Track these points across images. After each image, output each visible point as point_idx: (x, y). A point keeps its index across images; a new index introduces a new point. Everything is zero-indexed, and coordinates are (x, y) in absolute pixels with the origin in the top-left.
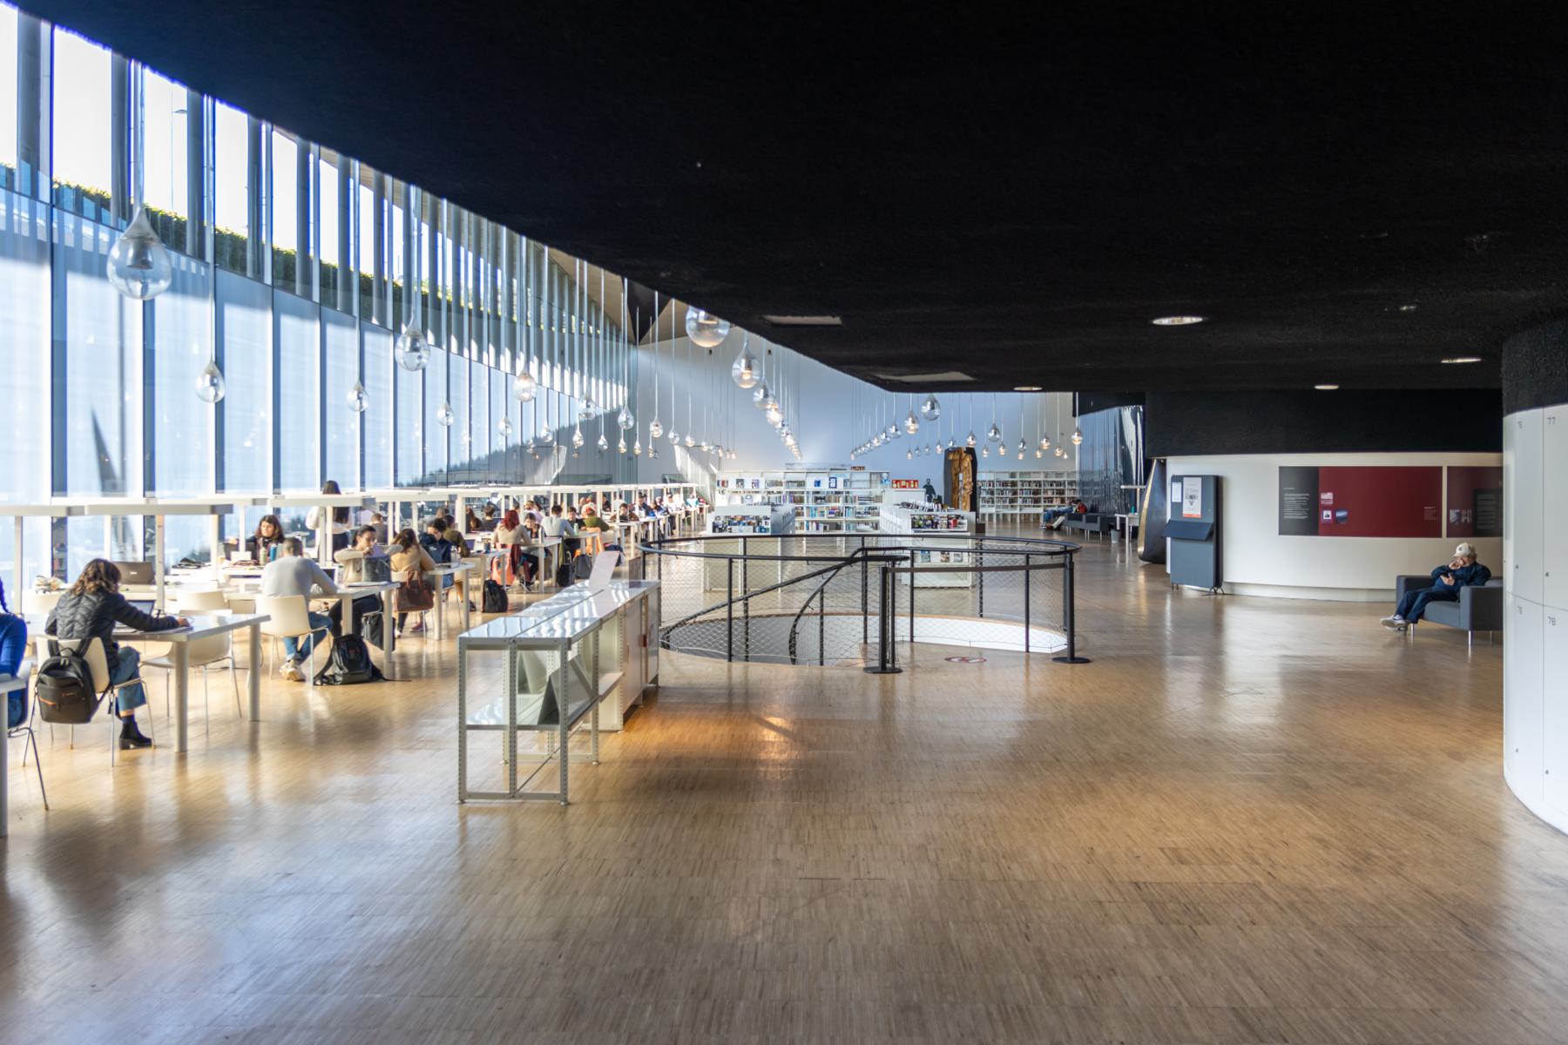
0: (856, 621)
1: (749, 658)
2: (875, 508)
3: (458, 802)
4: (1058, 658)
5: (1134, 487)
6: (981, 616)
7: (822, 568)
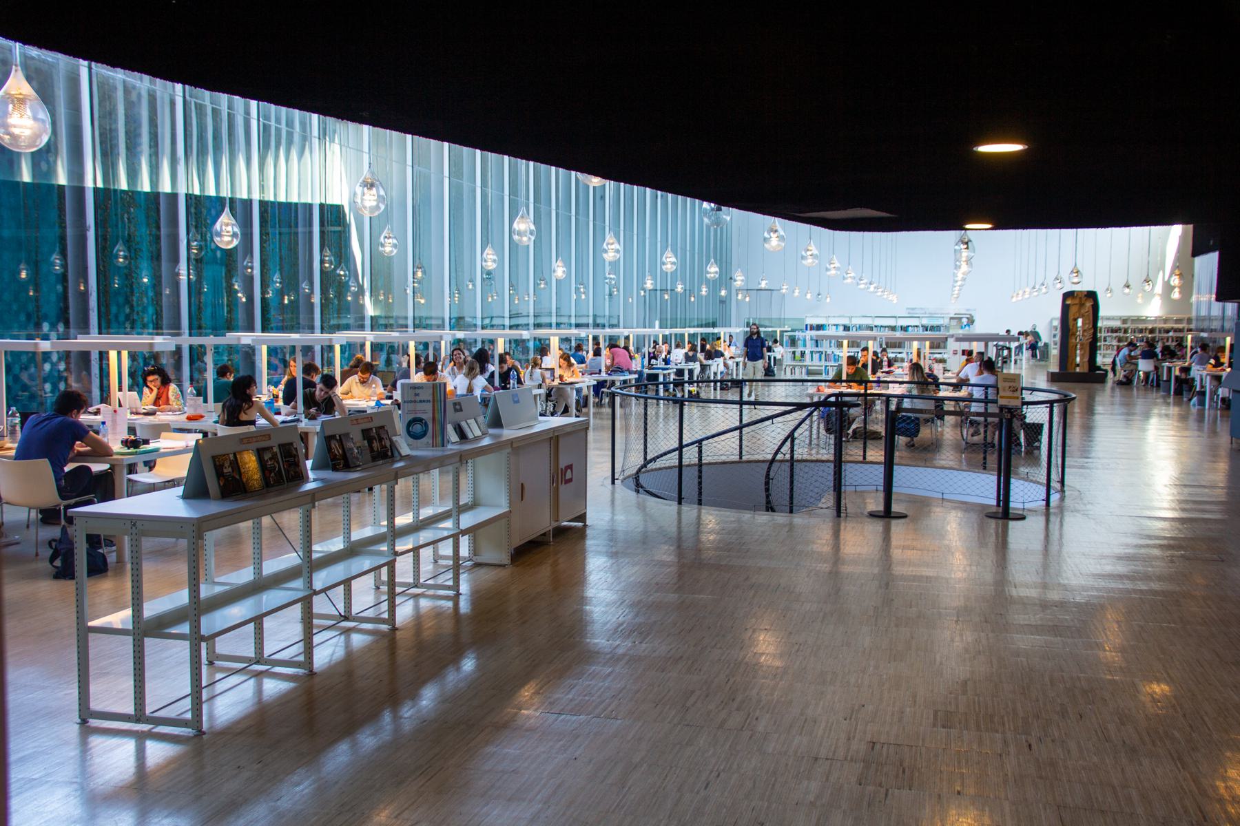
0: (826, 469)
1: (703, 501)
2: (403, 346)
3: (79, 721)
4: (196, 736)
5: (246, 338)
6: (985, 468)
7: (770, 413)
